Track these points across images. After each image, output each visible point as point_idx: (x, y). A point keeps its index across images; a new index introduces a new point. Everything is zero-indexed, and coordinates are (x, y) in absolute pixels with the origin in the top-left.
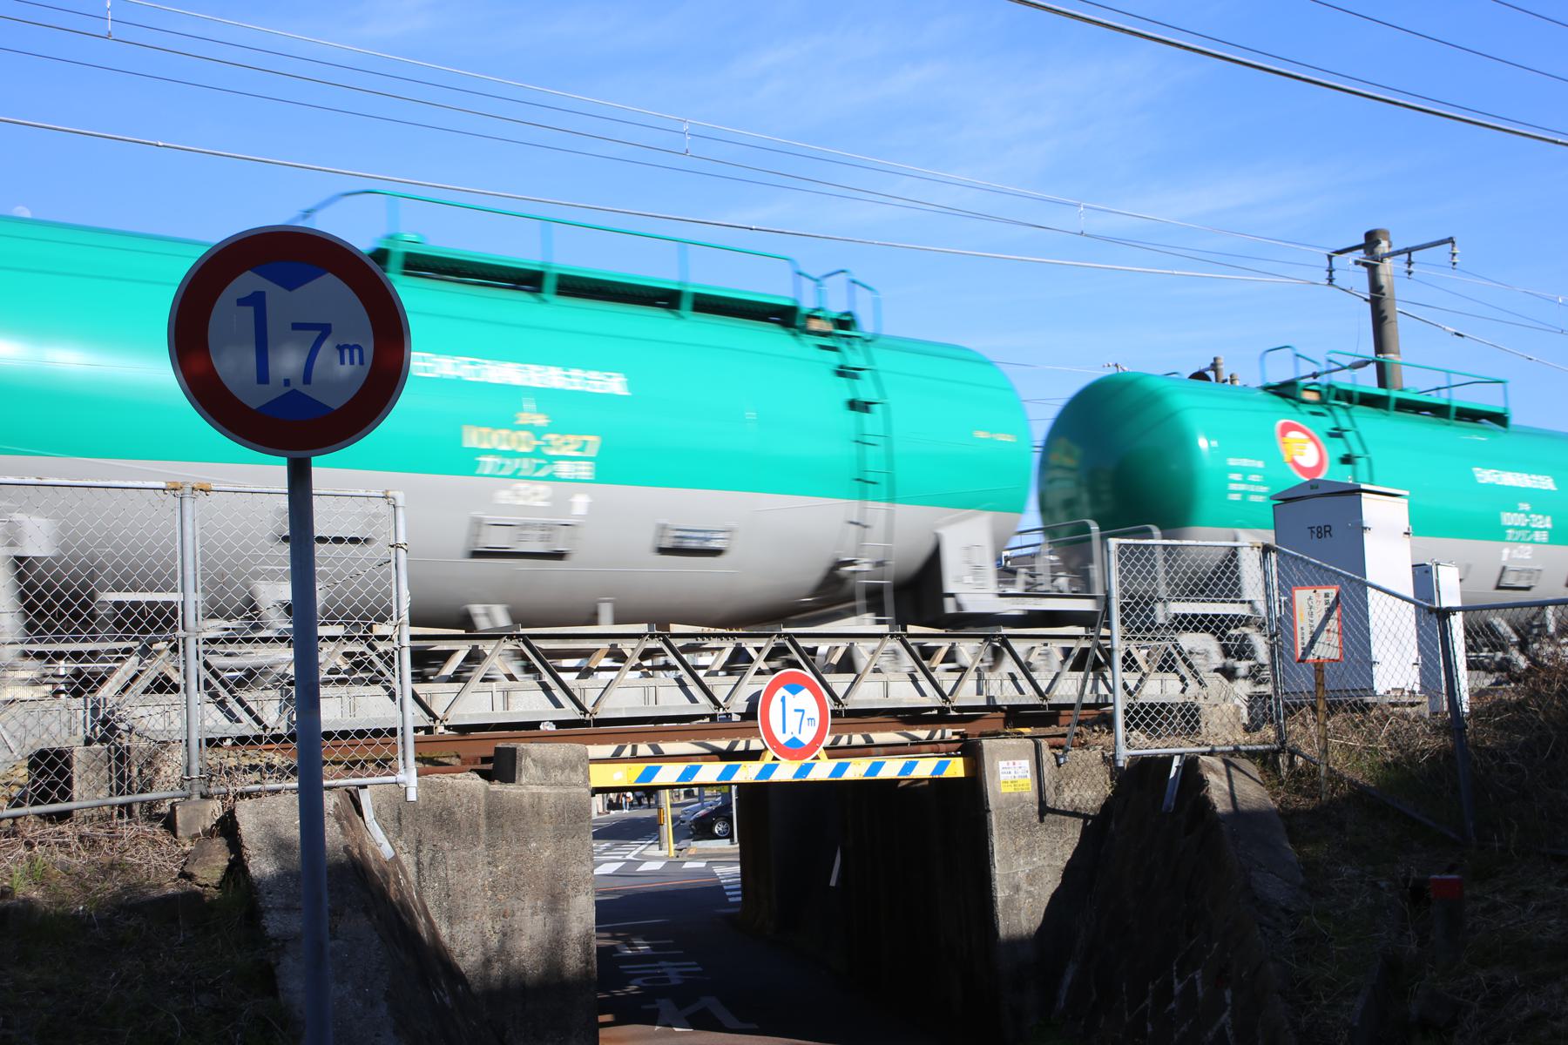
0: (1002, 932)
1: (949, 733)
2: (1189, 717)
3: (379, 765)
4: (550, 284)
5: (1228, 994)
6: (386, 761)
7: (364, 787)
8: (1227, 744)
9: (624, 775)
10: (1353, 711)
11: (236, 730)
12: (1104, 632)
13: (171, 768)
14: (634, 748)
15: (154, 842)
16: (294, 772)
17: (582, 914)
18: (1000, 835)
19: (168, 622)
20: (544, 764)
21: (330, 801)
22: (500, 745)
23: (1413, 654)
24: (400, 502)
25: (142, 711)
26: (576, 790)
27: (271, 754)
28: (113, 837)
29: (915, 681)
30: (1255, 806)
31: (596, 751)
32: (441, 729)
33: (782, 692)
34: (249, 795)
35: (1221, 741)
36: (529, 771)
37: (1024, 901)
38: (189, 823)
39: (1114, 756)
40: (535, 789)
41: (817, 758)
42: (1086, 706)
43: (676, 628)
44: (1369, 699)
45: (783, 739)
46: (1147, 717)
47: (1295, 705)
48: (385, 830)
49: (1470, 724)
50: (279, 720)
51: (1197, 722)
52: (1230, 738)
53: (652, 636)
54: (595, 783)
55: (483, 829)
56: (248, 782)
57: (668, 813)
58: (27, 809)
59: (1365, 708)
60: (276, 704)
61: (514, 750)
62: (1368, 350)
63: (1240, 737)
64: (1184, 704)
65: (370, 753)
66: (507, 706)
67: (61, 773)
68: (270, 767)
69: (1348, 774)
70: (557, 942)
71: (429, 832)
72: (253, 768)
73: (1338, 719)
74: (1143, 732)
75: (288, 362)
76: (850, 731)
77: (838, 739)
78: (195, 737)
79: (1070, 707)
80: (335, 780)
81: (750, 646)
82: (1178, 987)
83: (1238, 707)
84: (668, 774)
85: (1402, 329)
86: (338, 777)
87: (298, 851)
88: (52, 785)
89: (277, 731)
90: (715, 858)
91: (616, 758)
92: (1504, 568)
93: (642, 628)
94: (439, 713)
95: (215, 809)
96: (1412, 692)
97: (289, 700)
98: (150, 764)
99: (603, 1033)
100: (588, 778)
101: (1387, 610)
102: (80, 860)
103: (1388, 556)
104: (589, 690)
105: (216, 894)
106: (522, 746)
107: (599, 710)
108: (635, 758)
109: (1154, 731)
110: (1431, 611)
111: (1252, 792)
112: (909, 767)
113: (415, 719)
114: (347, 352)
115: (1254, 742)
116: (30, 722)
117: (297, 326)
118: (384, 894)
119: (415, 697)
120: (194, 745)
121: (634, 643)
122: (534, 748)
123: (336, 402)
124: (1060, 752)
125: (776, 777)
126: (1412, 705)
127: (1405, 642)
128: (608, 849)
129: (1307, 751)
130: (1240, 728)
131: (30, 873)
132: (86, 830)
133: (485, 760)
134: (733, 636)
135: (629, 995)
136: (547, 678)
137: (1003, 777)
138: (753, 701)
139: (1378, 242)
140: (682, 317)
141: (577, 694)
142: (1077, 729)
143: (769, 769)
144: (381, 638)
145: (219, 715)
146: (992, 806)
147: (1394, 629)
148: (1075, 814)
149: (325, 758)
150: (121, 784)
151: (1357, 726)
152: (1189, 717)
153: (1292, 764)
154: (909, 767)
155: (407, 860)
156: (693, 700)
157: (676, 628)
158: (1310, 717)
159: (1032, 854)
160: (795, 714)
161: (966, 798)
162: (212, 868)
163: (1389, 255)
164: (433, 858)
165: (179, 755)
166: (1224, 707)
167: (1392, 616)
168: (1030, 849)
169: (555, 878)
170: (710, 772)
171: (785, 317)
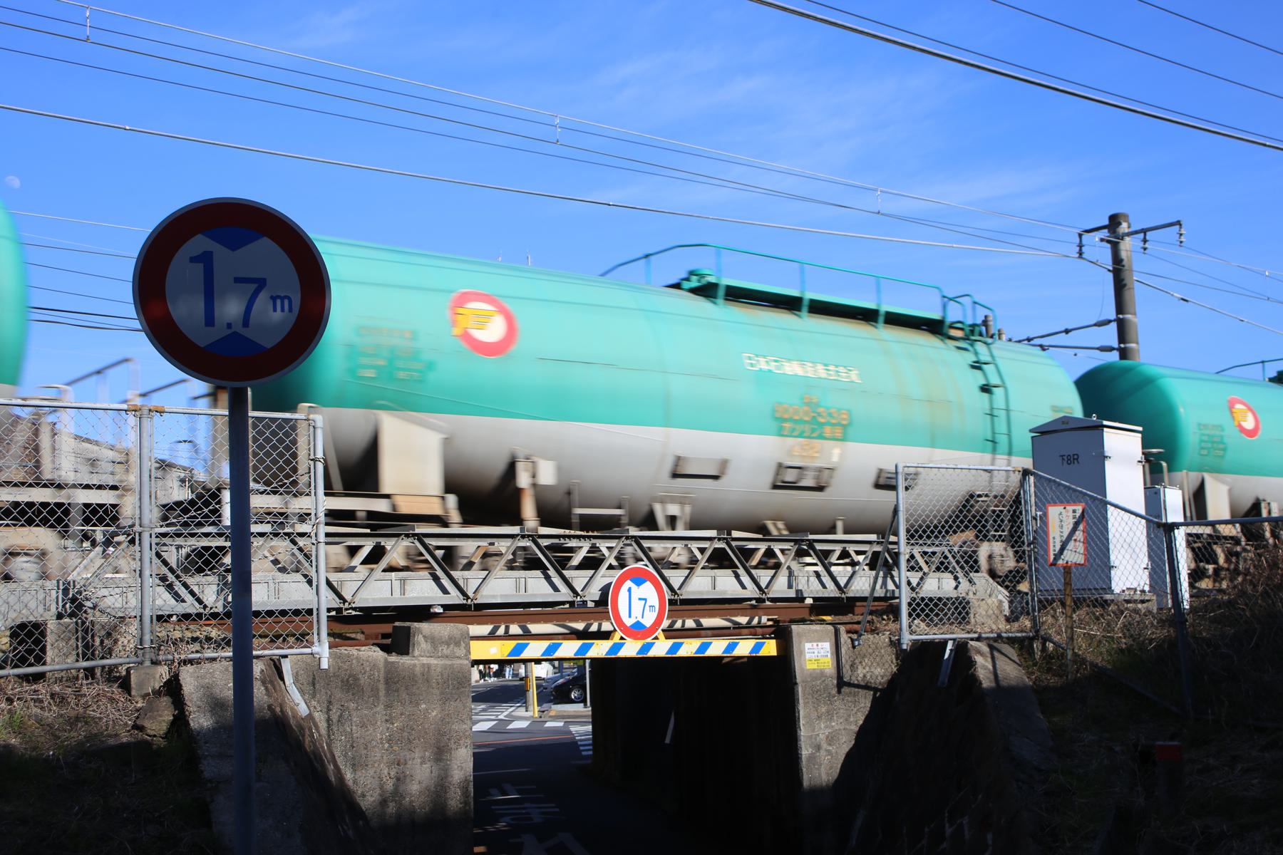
0: (806, 783)
2: (960, 609)
3: (297, 639)
5: (989, 836)
6: (303, 635)
7: (286, 656)
10: (1095, 606)
11: (181, 609)
12: (892, 539)
13: (127, 639)
14: (507, 628)
15: (112, 700)
16: (228, 644)
17: (462, 764)
18: (805, 704)
20: (431, 639)
21: (258, 668)
23: (1145, 561)
25: (104, 592)
27: (209, 629)
28: (78, 695)
30: (1013, 683)
31: (476, 630)
33: (628, 584)
34: (191, 662)
35: (987, 629)
37: (824, 758)
38: (141, 684)
39: (899, 640)
40: (425, 660)
41: (656, 638)
44: (1108, 597)
45: (629, 622)
46: (926, 608)
47: (1047, 600)
48: (302, 692)
49: (1190, 618)
51: (967, 613)
52: (994, 627)
53: (523, 537)
54: (474, 656)
55: (382, 693)
56: (189, 652)
60: (215, 588)
62: (1112, 315)
63: (1003, 626)
64: (957, 599)
65: (291, 628)
66: (403, 592)
67: (37, 642)
68: (208, 639)
69: (1089, 657)
70: (441, 786)
71: (338, 694)
72: (195, 640)
73: (1082, 612)
74: (923, 621)
75: (231, 309)
78: (147, 613)
79: (864, 599)
80: (262, 651)
81: (603, 545)
82: (949, 830)
83: (1001, 602)
85: (1139, 294)
87: (231, 710)
88: (30, 652)
90: (571, 719)
91: (492, 636)
94: (348, 597)
95: (163, 673)
96: (1143, 591)
97: (226, 584)
98: (109, 635)
100: (469, 652)
101: (1123, 524)
102: (51, 713)
105: (162, 743)
108: (508, 636)
110: (1159, 525)
111: (1011, 670)
112: (731, 647)
113: (328, 601)
114: (279, 302)
115: (1013, 630)
116: (12, 600)
118: (299, 745)
119: (329, 583)
120: (147, 620)
121: (508, 542)
123: (269, 342)
124: (855, 636)
126: (1143, 602)
127: (1137, 550)
128: (484, 710)
129: (1057, 638)
130: (1003, 619)
132: (57, 688)
133: (385, 636)
134: (589, 537)
135: (499, 831)
137: (808, 656)
138: (605, 590)
141: (461, 583)
142: (869, 618)
143: (617, 647)
144: (302, 535)
145: (167, 596)
146: (799, 680)
147: (1128, 540)
148: (866, 687)
150: (88, 651)
151: (1097, 619)
152: (960, 609)
153: (1044, 649)
154: (731, 647)
155: (320, 717)
156: (556, 589)
157: (736, 534)
159: (831, 720)
161: (780, 670)
162: (159, 722)
163: (1129, 234)
164: (341, 716)
165: (133, 628)
166: (989, 601)
167: (1127, 529)
170: (569, 649)
171: (934, 327)
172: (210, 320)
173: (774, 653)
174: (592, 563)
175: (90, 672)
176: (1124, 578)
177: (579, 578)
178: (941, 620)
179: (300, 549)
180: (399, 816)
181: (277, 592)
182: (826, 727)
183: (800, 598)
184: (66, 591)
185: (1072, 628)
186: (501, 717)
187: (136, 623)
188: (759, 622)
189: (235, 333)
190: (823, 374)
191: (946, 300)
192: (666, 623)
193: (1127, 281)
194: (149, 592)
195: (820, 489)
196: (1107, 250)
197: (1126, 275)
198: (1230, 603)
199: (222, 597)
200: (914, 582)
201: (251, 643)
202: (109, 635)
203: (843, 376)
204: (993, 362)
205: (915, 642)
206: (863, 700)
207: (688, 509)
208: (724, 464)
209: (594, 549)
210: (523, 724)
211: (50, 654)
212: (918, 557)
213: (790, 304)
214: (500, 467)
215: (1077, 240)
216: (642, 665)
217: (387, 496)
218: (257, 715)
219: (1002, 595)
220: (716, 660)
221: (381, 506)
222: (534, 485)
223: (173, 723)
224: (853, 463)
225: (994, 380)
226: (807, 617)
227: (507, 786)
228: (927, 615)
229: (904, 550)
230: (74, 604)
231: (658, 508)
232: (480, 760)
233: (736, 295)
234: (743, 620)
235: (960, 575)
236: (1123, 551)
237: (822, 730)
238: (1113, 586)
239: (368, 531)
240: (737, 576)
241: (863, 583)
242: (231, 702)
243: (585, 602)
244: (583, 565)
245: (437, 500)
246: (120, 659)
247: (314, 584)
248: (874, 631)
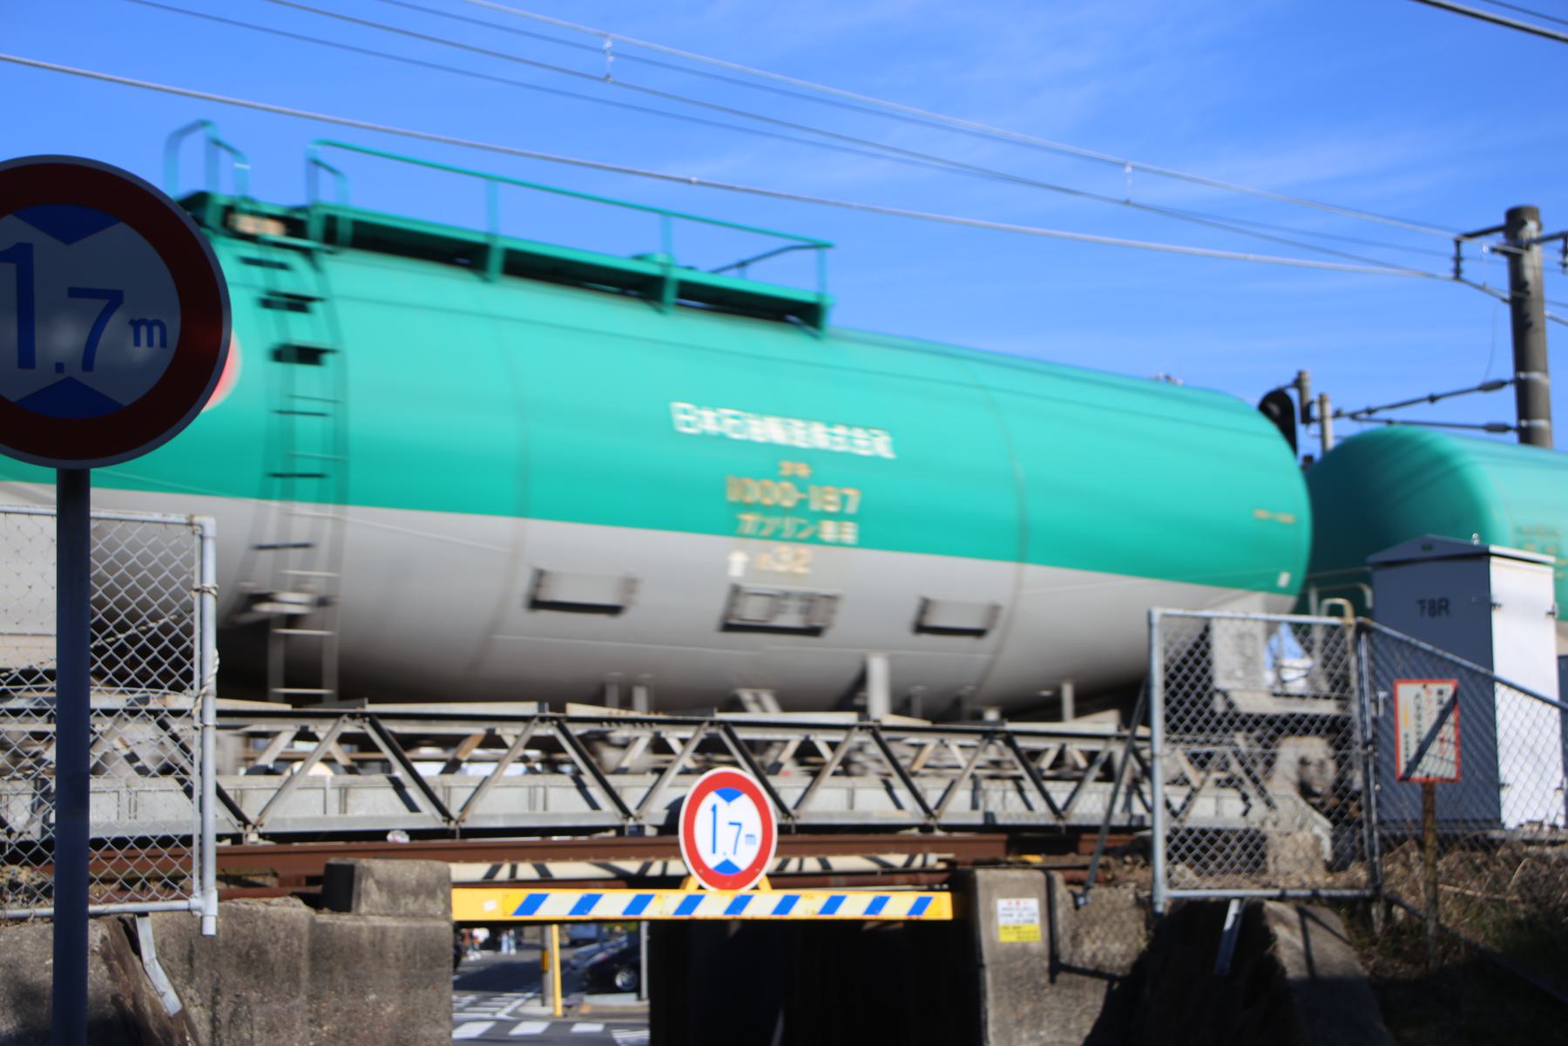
1: (932, 859)
2: (1251, 849)
3: (166, 885)
4: (496, 261)
6: (176, 878)
7: (144, 914)
8: (1303, 886)
9: (497, 905)
10: (1473, 849)
12: (1142, 731)
14: (514, 870)
16: (47, 893)
18: (998, 999)
20: (391, 888)
21: (96, 933)
22: (333, 860)
24: (210, 530)
26: (432, 924)
27: (16, 868)
29: (889, 789)
30: (1338, 972)
32: (253, 838)
33: (713, 798)
35: (1294, 883)
36: (371, 897)
39: (1151, 897)
40: (377, 921)
41: (756, 888)
42: (1116, 830)
43: (575, 710)
44: (1495, 834)
45: (712, 861)
46: (1196, 846)
47: (1394, 837)
50: (31, 821)
51: (1263, 856)
52: (1306, 879)
53: (543, 720)
54: (460, 914)
55: (305, 974)
59: (1490, 846)
60: (27, 800)
61: (351, 868)
62: (1506, 370)
63: (1321, 878)
64: (1246, 831)
65: (154, 867)
66: (344, 807)
69: (1464, 933)
71: (231, 977)
73: (1452, 859)
74: (1191, 866)
75: (63, 339)
76: (802, 851)
77: (784, 863)
79: (1093, 829)
80: (103, 904)
81: (673, 736)
83: (1318, 839)
84: (558, 904)
86: (109, 901)
87: (48, 1003)
89: (29, 838)
91: (488, 882)
93: (529, 708)
94: (252, 816)
96: (1554, 827)
97: (46, 794)
100: (449, 907)
101: (1521, 715)
104: (456, 792)
106: (364, 862)
107: (468, 816)
108: (514, 883)
109: (1205, 866)
111: (1334, 951)
112: (878, 904)
113: (218, 823)
114: (143, 330)
115: (1337, 884)
117: (74, 293)
119: (221, 793)
121: (518, 728)
122: (380, 866)
123: (126, 395)
124: (1079, 890)
125: (703, 912)
126: (1554, 843)
127: (1545, 758)
128: (473, 1004)
129: (1410, 900)
130: (1320, 866)
133: (312, 880)
134: (650, 722)
136: (399, 772)
137: (1002, 921)
138: (674, 808)
139: (1524, 223)
140: (487, 280)
141: (439, 794)
142: (1102, 860)
143: (692, 902)
144: (177, 713)
146: (987, 957)
147: (1530, 741)
148: (1097, 973)
149: (92, 874)
151: (1478, 869)
153: (1389, 917)
154: (878, 904)
155: (199, 1015)
156: (594, 806)
158: (1414, 854)
159: (1039, 1026)
160: (729, 830)
161: (953, 949)
163: (1539, 241)
164: (235, 1013)
166: (1300, 836)
167: (1528, 723)
170: (613, 904)
176: (1522, 805)
178: (1220, 865)
179: (175, 737)
181: (134, 807)
182: (1031, 1038)
185: (1435, 884)
186: (502, 1015)
188: (924, 864)
189: (70, 381)
192: (772, 864)
193: (1534, 318)
195: (814, 631)
197: (1532, 308)
199: (39, 816)
200: (1177, 802)
201: (87, 892)
205: (1177, 902)
206: (1090, 995)
210: (536, 1028)
215: (1452, 250)
219: (1321, 827)
220: (854, 925)
226: (1001, 857)
228: (1197, 858)
234: (898, 860)
236: (1521, 760)
238: (1505, 816)
239: (288, 708)
241: (1092, 804)
242: (48, 992)
243: (640, 828)
247: (196, 794)
248: (1111, 882)
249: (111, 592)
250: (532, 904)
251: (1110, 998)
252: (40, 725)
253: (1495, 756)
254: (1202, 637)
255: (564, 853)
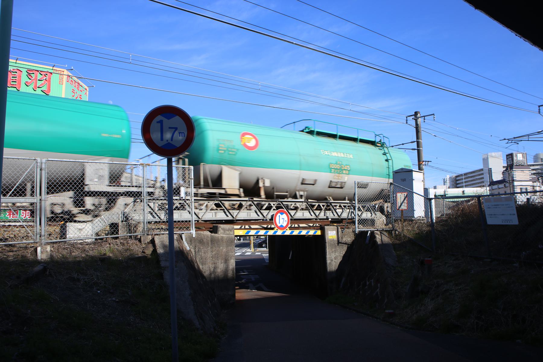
0: (328, 270)
1: (317, 225)
2: (372, 222)
5: (379, 285)
6: (188, 228)
9: (242, 233)
11: (155, 220)
12: (354, 202)
13: (140, 229)
15: (136, 245)
17: (232, 264)
19: (140, 195)
20: (223, 229)
21: (175, 237)
23: (423, 209)
25: (134, 215)
28: (128, 243)
31: (236, 227)
33: (279, 214)
34: (157, 235)
36: (221, 231)
37: (334, 263)
38: (144, 241)
40: (222, 235)
45: (279, 225)
46: (363, 222)
48: (188, 243)
49: (435, 225)
54: (236, 234)
56: (157, 232)
57: (252, 242)
58: (109, 236)
59: (412, 221)
63: (384, 227)
67: (116, 228)
68: (162, 228)
69: (408, 235)
70: (226, 270)
71: (198, 244)
72: (158, 228)
73: (406, 223)
75: (168, 136)
78: (145, 221)
79: (345, 219)
80: (176, 232)
81: (272, 203)
82: (368, 283)
84: (253, 232)
85: (423, 134)
88: (115, 231)
90: (263, 252)
91: (240, 229)
92: (331, 181)
94: (200, 217)
95: (150, 237)
98: (135, 227)
99: (236, 291)
102: (121, 248)
103: (418, 187)
105: (150, 257)
106: (219, 225)
108: (245, 229)
110: (428, 199)
111: (386, 239)
112: (308, 232)
116: (110, 217)
117: (170, 128)
118: (187, 258)
119: (195, 213)
120: (145, 223)
123: (178, 145)
125: (277, 234)
129: (399, 230)
131: (110, 250)
132: (122, 241)
133: (211, 228)
135: (243, 283)
138: (272, 216)
144: (187, 200)
145: (151, 216)
148: (346, 244)
150: (130, 231)
152: (372, 222)
154: (308, 232)
155: (193, 250)
156: (258, 216)
157: (309, 200)
160: (282, 219)
161: (321, 240)
162: (149, 251)
165: (142, 225)
168: (335, 251)
169: (226, 256)
170: (262, 232)
171: (373, 143)
172: (162, 139)
173: (320, 234)
174: (269, 208)
175: (131, 237)
177: (265, 213)
180: (215, 278)
183: (327, 219)
184: (124, 215)
187: (142, 224)
190: (343, 156)
191: (376, 135)
192: (289, 226)
194: (146, 215)
195: (342, 188)
196: (414, 121)
197: (419, 128)
198: (446, 221)
202: (135, 227)
203: (348, 156)
204: (389, 153)
207: (305, 193)
208: (316, 181)
209: (269, 204)
210: (249, 254)
211: (120, 232)
212: (361, 207)
213: (334, 136)
214: (254, 181)
216: (283, 237)
217: (224, 189)
218: (175, 249)
219: (384, 218)
221: (222, 191)
222: (264, 186)
223: (153, 251)
224: (350, 180)
225: (389, 158)
227: (245, 270)
229: (357, 205)
230: (126, 218)
231: (297, 193)
232: (237, 263)
233: (319, 134)
234: (311, 225)
235: (372, 212)
237: (333, 256)
240: (310, 212)
244: (266, 209)
245: (238, 190)
246: (139, 233)
249: (7, 177)
250: (248, 232)
251: (348, 248)
252: (165, 202)
253: (486, 218)
254: (82, 177)
255: (253, 224)
